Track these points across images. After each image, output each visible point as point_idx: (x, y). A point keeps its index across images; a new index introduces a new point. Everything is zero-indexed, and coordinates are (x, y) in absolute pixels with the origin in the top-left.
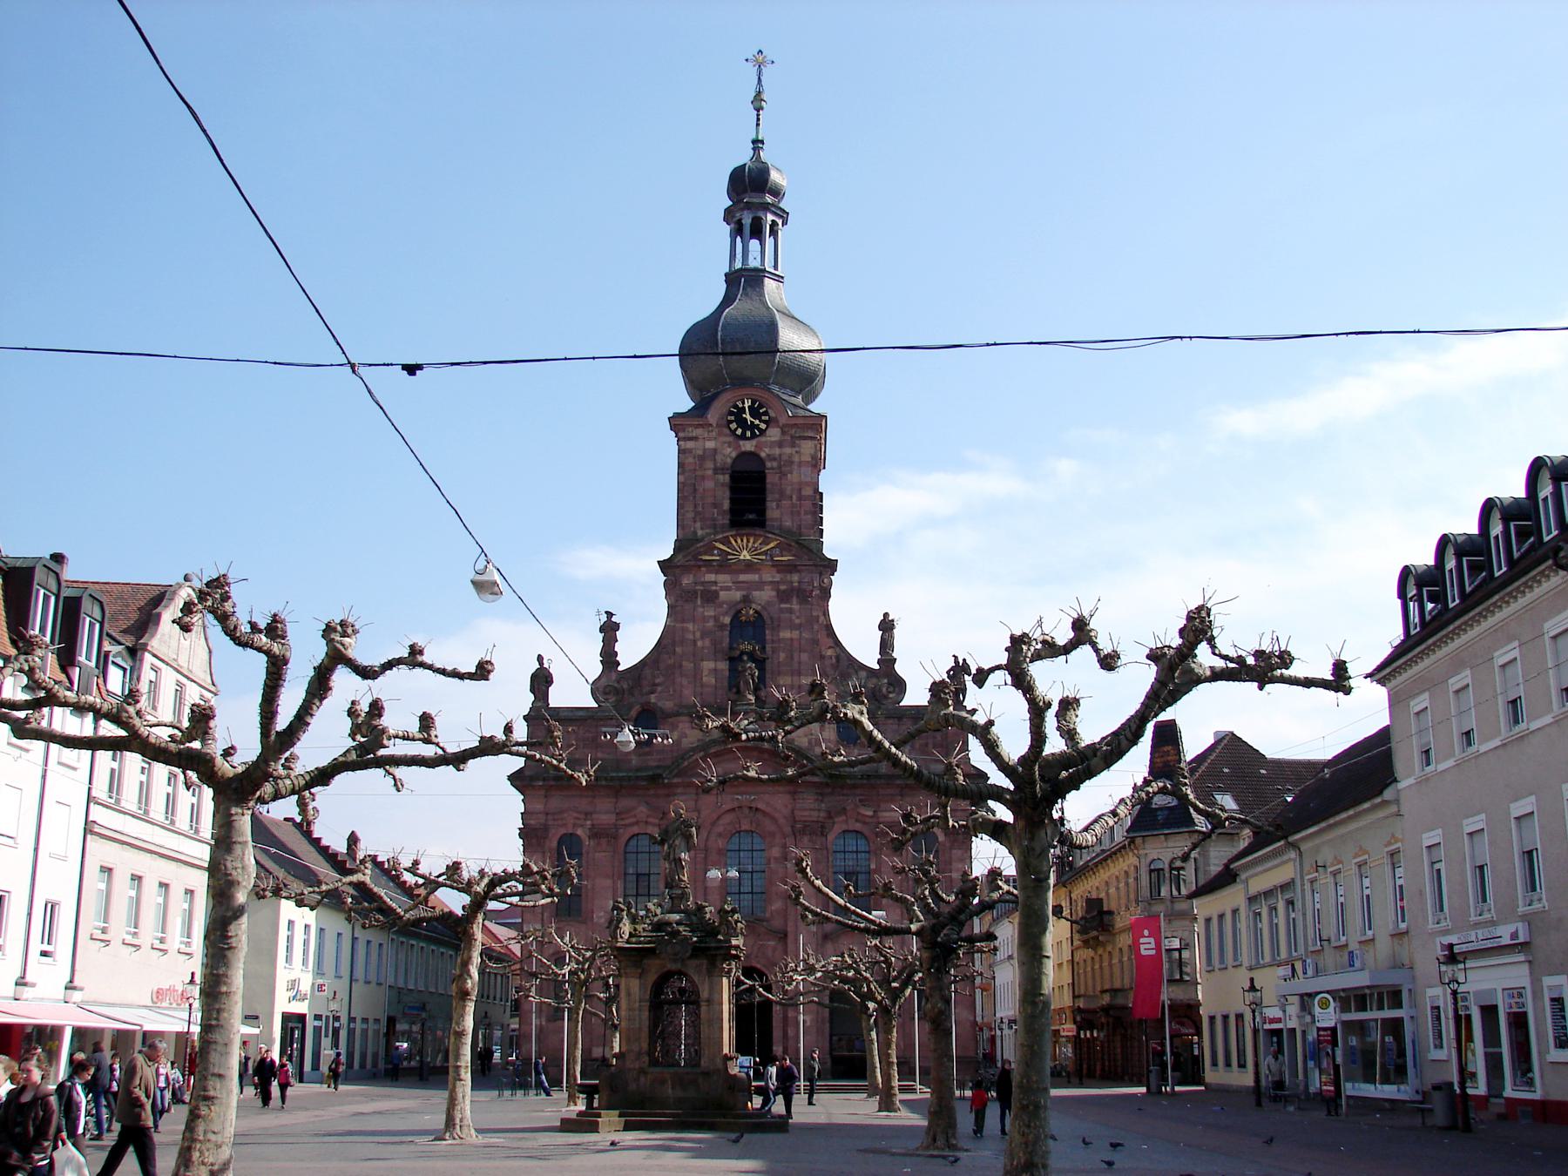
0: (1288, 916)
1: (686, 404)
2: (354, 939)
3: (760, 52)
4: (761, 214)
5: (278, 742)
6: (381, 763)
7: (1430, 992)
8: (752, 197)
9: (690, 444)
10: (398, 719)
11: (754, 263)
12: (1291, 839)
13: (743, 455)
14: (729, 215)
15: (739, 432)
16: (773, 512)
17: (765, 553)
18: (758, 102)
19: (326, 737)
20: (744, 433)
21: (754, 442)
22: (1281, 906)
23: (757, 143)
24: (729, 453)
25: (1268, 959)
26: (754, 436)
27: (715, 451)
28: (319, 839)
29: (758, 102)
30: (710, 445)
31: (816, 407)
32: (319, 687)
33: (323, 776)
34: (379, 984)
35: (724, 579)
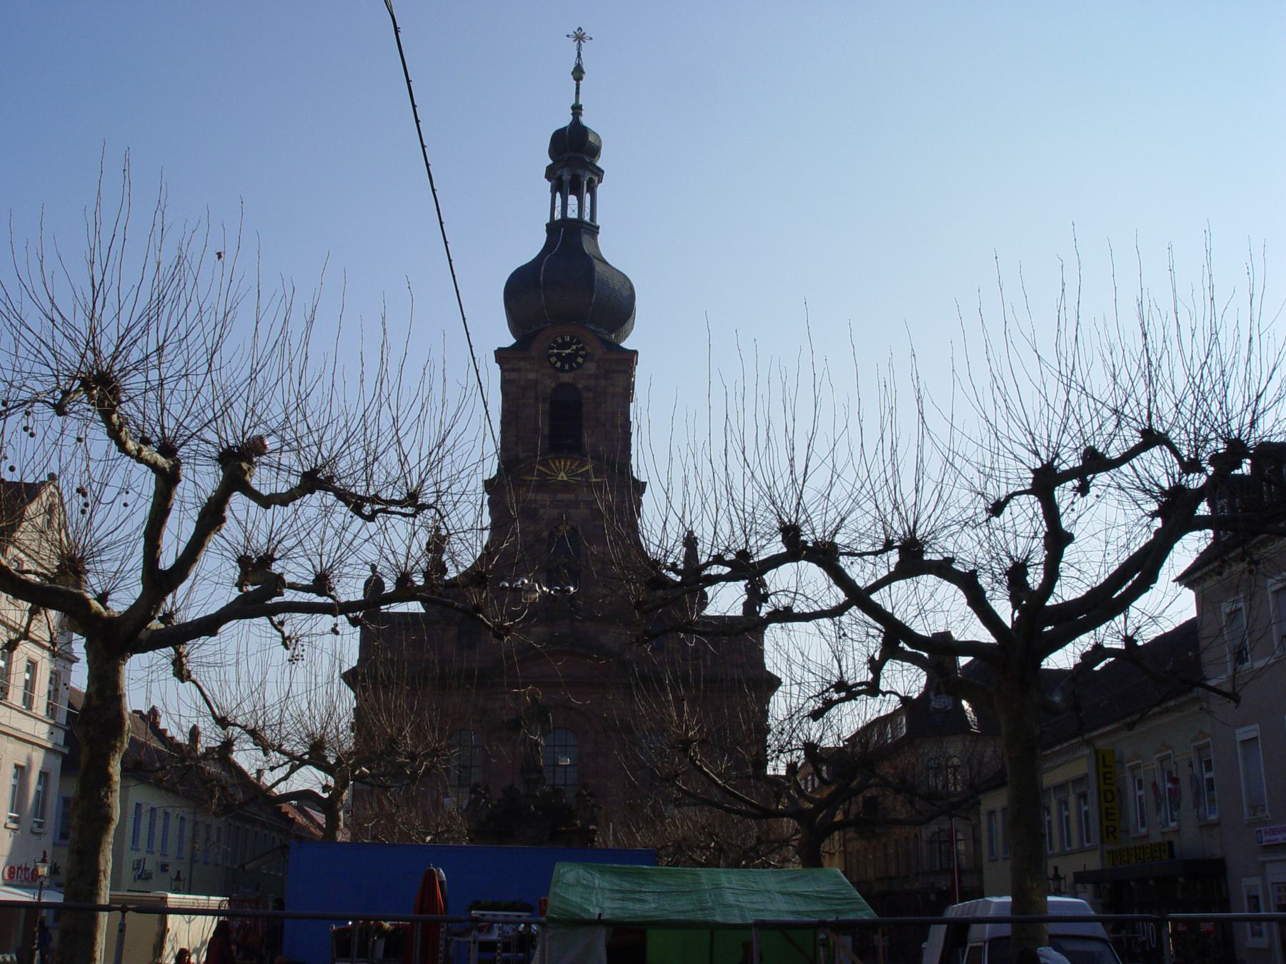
0: (1079, 808)
1: (508, 340)
2: (196, 823)
3: (580, 29)
4: (579, 172)
5: (160, 582)
6: (270, 612)
7: (1247, 882)
8: (574, 158)
9: (514, 375)
10: (296, 570)
11: (572, 214)
12: (1086, 736)
13: (561, 386)
14: (550, 173)
15: (559, 364)
16: (587, 439)
17: (581, 475)
18: (578, 73)
19: (210, 586)
20: (563, 366)
21: (572, 375)
22: (1072, 800)
23: (577, 109)
24: (549, 384)
25: (1075, 845)
26: (571, 369)
27: (536, 382)
28: (165, 730)
29: (578, 73)
30: (532, 376)
31: (627, 344)
32: (212, 517)
33: (209, 626)
34: (217, 865)
35: (543, 498)
